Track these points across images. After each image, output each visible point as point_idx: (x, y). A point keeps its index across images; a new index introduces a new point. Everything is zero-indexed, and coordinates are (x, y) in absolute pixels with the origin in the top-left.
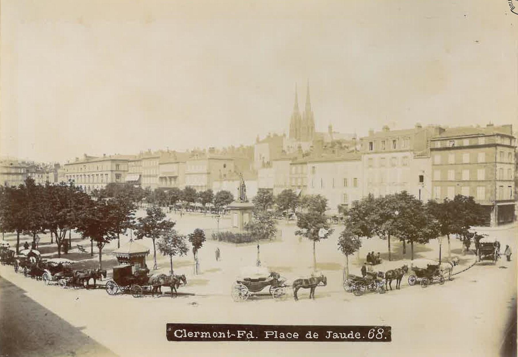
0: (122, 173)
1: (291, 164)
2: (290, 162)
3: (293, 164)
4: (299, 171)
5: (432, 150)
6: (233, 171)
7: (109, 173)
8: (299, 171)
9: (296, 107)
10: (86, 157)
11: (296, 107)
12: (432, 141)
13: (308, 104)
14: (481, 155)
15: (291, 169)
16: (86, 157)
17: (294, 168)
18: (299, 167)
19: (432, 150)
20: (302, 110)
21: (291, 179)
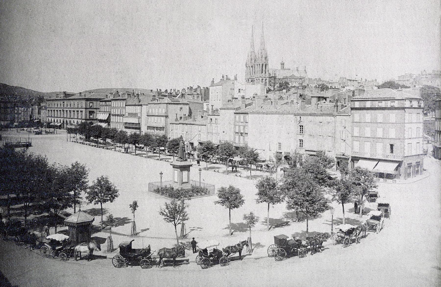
0: (95, 110)
1: (235, 113)
2: (234, 111)
3: (237, 113)
4: (237, 127)
5: (352, 109)
6: (187, 115)
7: (84, 110)
8: (237, 127)
9: (253, 46)
10: (65, 94)
11: (253, 46)
12: (352, 101)
13: (263, 43)
14: (393, 116)
15: (235, 117)
16: (65, 94)
17: (237, 116)
18: (242, 116)
19: (352, 109)
20: (257, 49)
21: (235, 125)
